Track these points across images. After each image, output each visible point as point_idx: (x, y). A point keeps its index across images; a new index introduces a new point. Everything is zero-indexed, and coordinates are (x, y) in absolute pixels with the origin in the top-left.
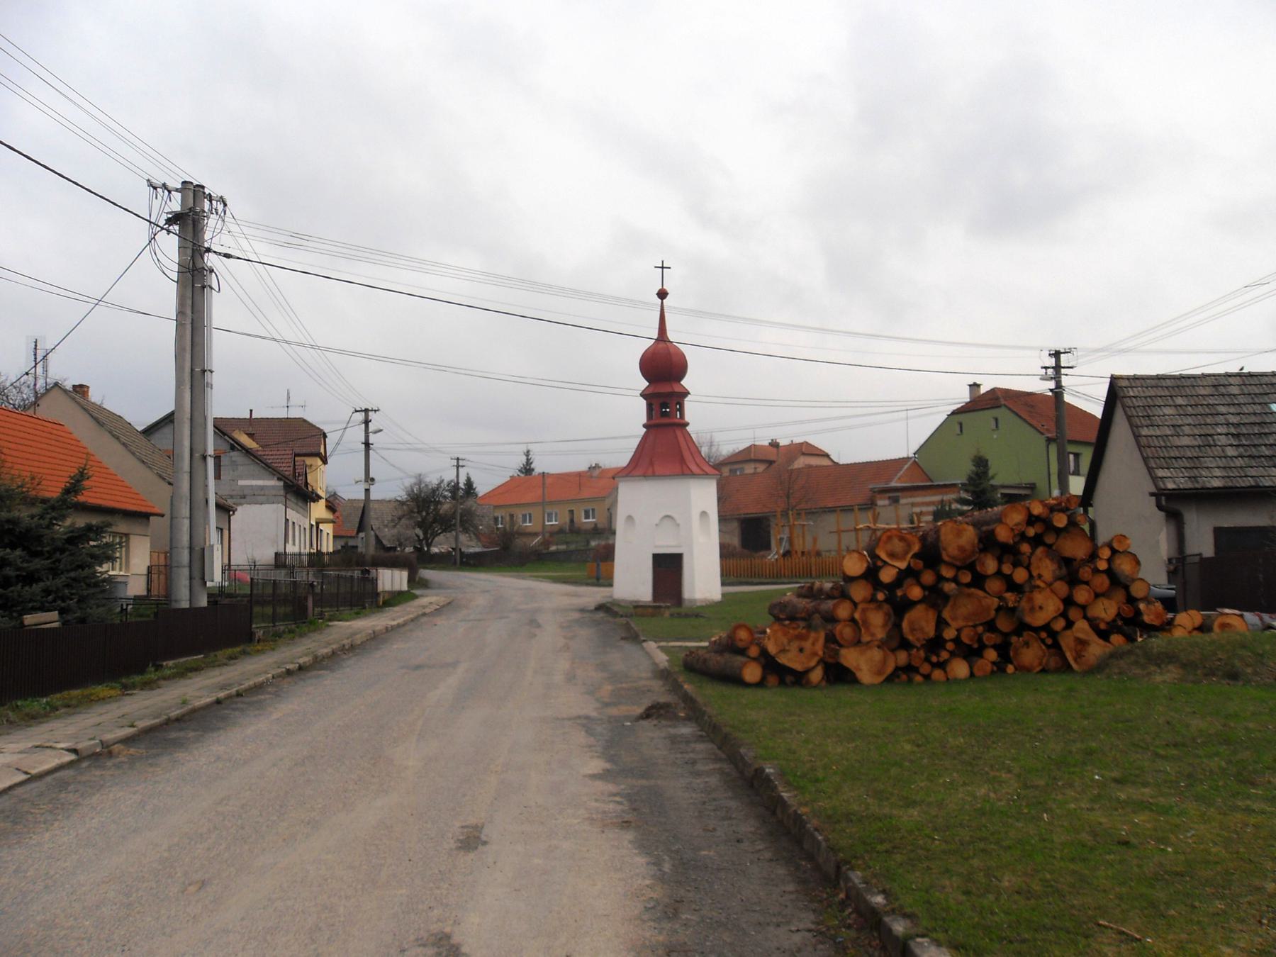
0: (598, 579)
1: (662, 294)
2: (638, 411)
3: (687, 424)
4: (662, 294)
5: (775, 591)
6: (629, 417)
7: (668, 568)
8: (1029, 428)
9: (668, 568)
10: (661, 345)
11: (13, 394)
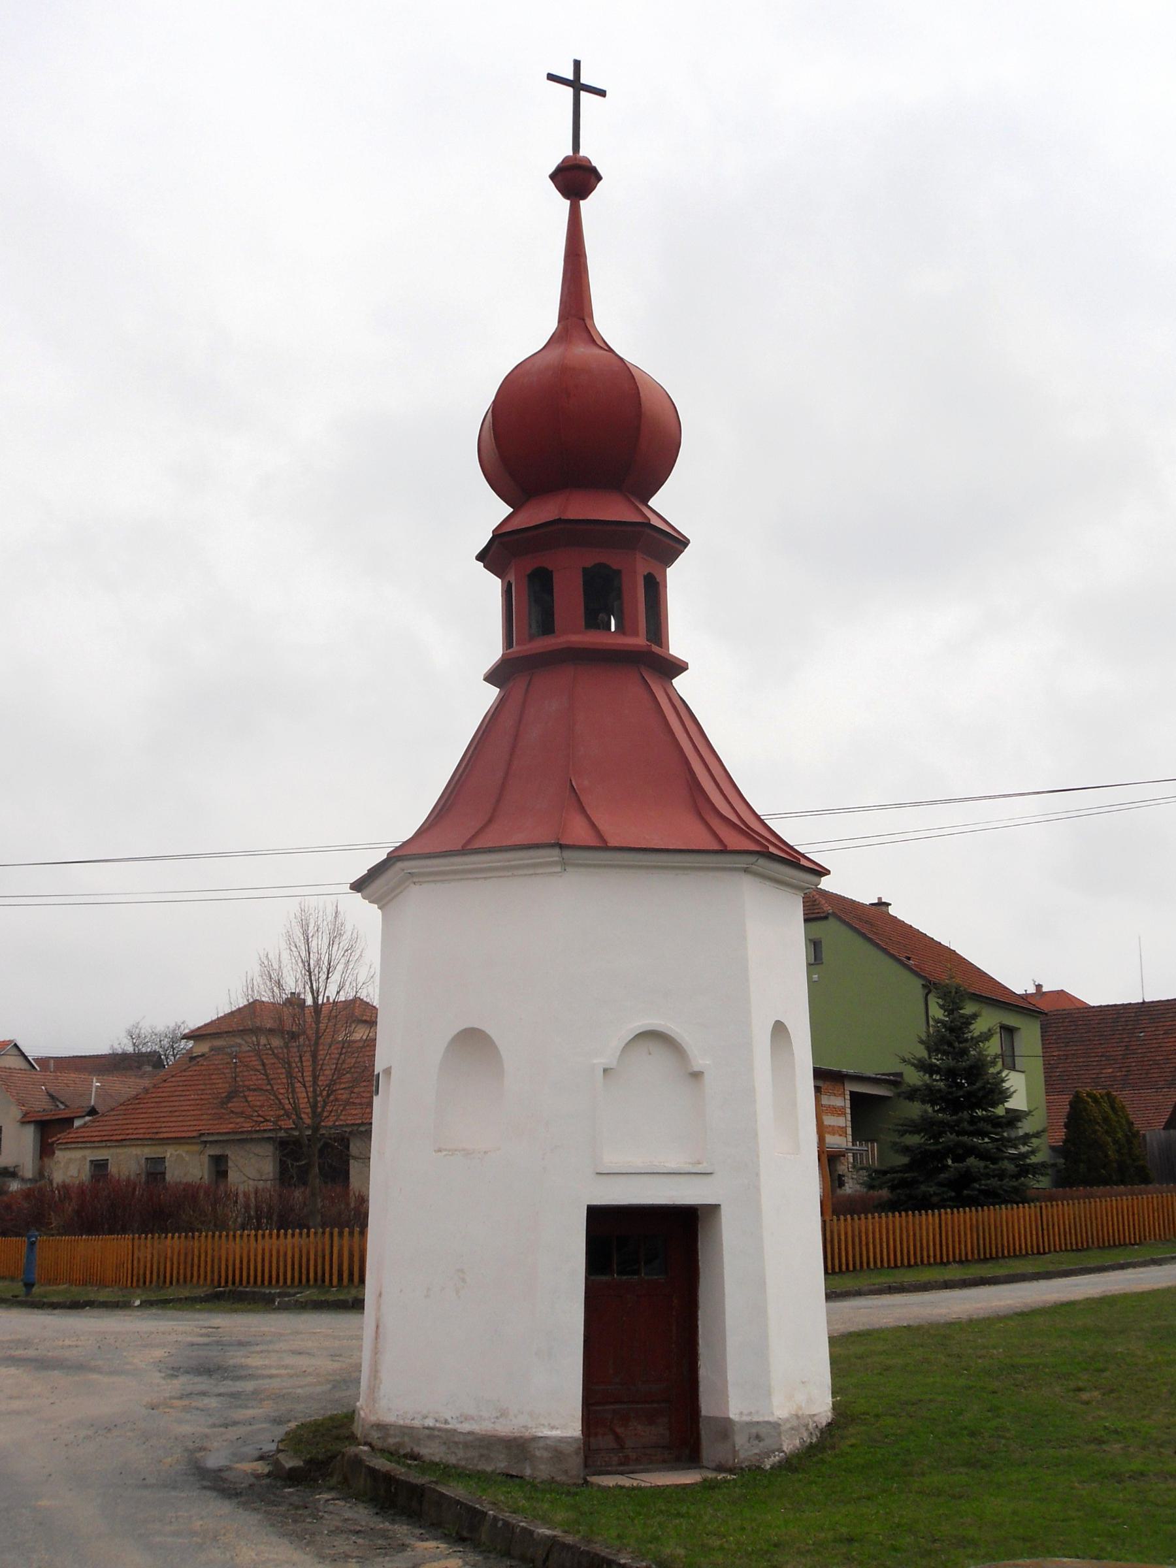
0: (29, 1285)
1: (576, 179)
2: (469, 622)
3: (679, 667)
4: (576, 179)
5: (1025, 1315)
6: (438, 644)
7: (647, 1264)
8: (844, 928)
9: (647, 1264)
10: (581, 351)
11: (740, 1440)
